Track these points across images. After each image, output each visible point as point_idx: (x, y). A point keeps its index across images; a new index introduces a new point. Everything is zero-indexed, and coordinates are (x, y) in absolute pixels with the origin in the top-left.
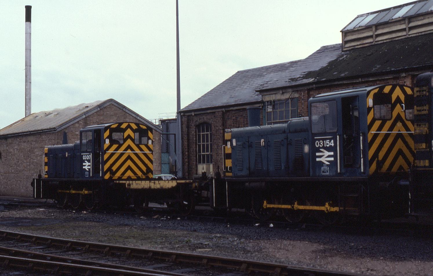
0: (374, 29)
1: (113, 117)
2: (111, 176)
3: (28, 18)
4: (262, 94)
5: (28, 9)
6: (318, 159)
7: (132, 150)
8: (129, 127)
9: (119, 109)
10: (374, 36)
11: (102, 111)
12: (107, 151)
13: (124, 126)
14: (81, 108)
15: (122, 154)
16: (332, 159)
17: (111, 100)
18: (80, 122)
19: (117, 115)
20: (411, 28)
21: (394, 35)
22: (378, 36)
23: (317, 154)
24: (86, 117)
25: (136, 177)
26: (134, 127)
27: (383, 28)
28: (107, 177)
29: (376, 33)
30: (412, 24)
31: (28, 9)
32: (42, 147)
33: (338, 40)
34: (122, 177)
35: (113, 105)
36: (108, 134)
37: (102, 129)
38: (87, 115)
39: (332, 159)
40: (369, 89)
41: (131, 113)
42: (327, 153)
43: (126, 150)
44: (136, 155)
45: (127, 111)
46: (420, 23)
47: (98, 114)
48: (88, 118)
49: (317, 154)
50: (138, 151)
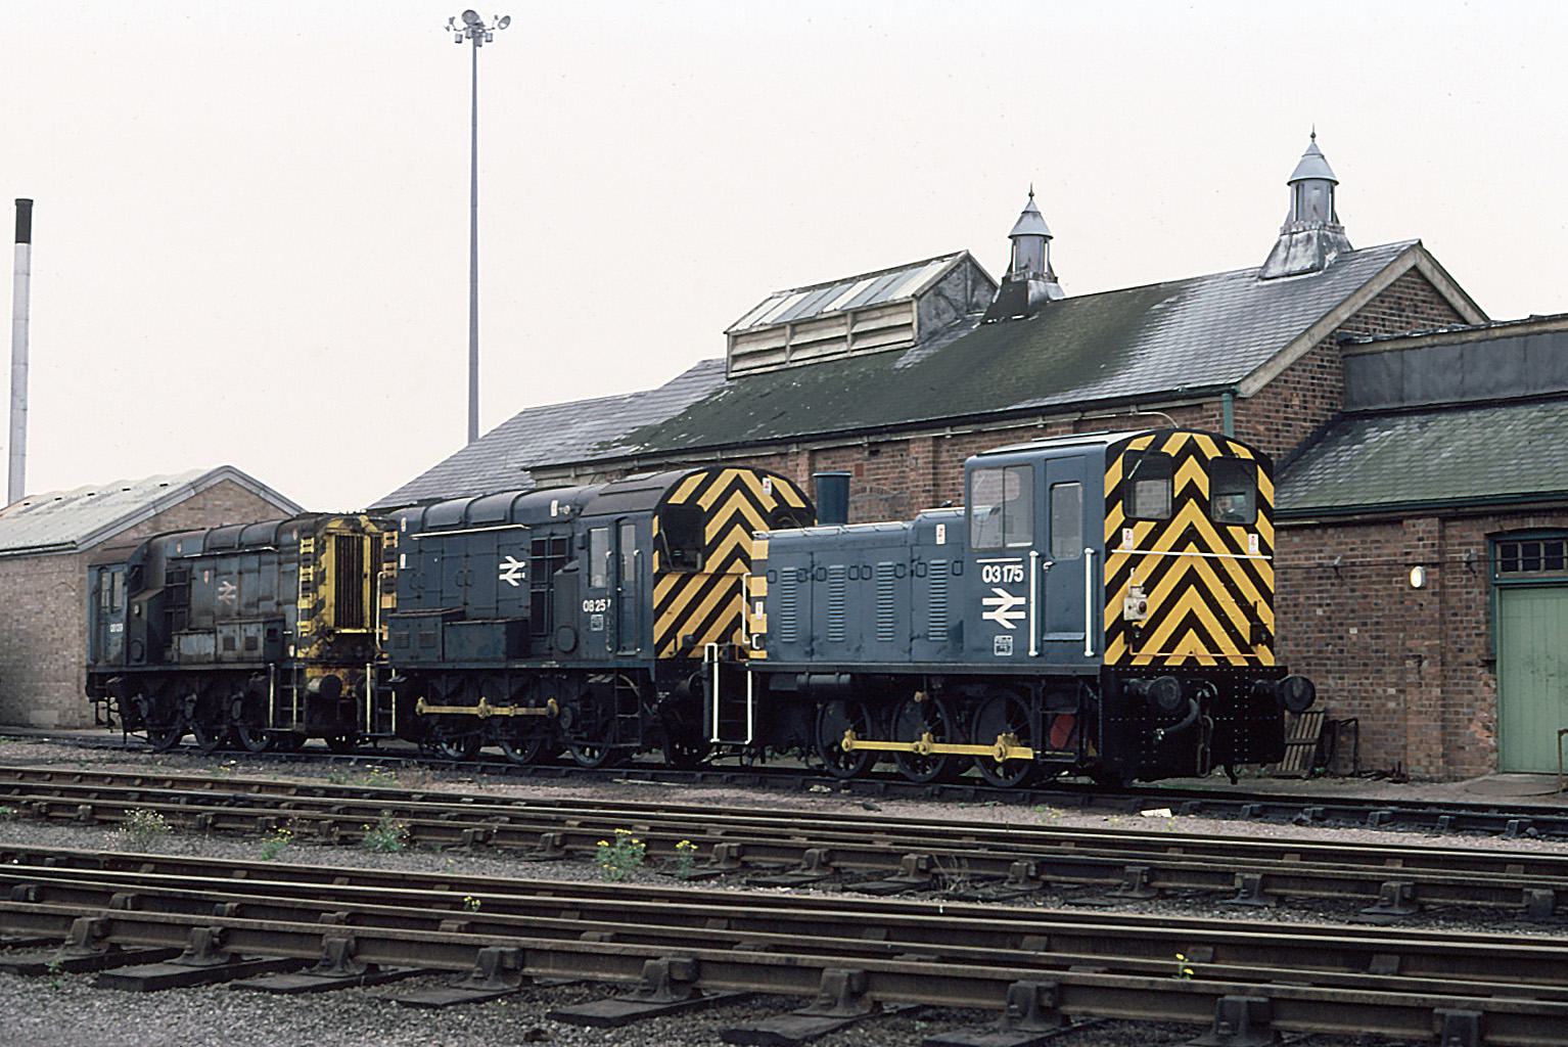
0: (788, 331)
1: (232, 513)
2: (1127, 650)
3: (23, 233)
4: (537, 476)
5: (24, 208)
6: (986, 616)
7: (1203, 546)
8: (1191, 449)
9: (247, 493)
10: (788, 348)
11: (201, 498)
12: (1116, 548)
13: (1173, 446)
14: (149, 487)
15: (1167, 563)
16: (1021, 615)
17: (228, 469)
18: (141, 527)
19: (243, 510)
20: (857, 336)
21: (827, 349)
22: (795, 348)
23: (986, 602)
24: (157, 514)
25: (1216, 658)
26: (1211, 451)
27: (807, 332)
28: (1112, 656)
29: (854, 331)
30: (797, 341)
31: (24, 208)
32: (41, 592)
33: (719, 351)
34: (1167, 658)
35: (232, 482)
36: (792, 505)
37: (1096, 454)
38: (160, 509)
39: (1021, 615)
40: (678, 474)
41: (279, 505)
42: (1008, 600)
43: (1180, 545)
44: (1215, 564)
45: (270, 499)
46: (872, 326)
47: (191, 506)
48: (163, 518)
49: (986, 602)
50: (1221, 552)
